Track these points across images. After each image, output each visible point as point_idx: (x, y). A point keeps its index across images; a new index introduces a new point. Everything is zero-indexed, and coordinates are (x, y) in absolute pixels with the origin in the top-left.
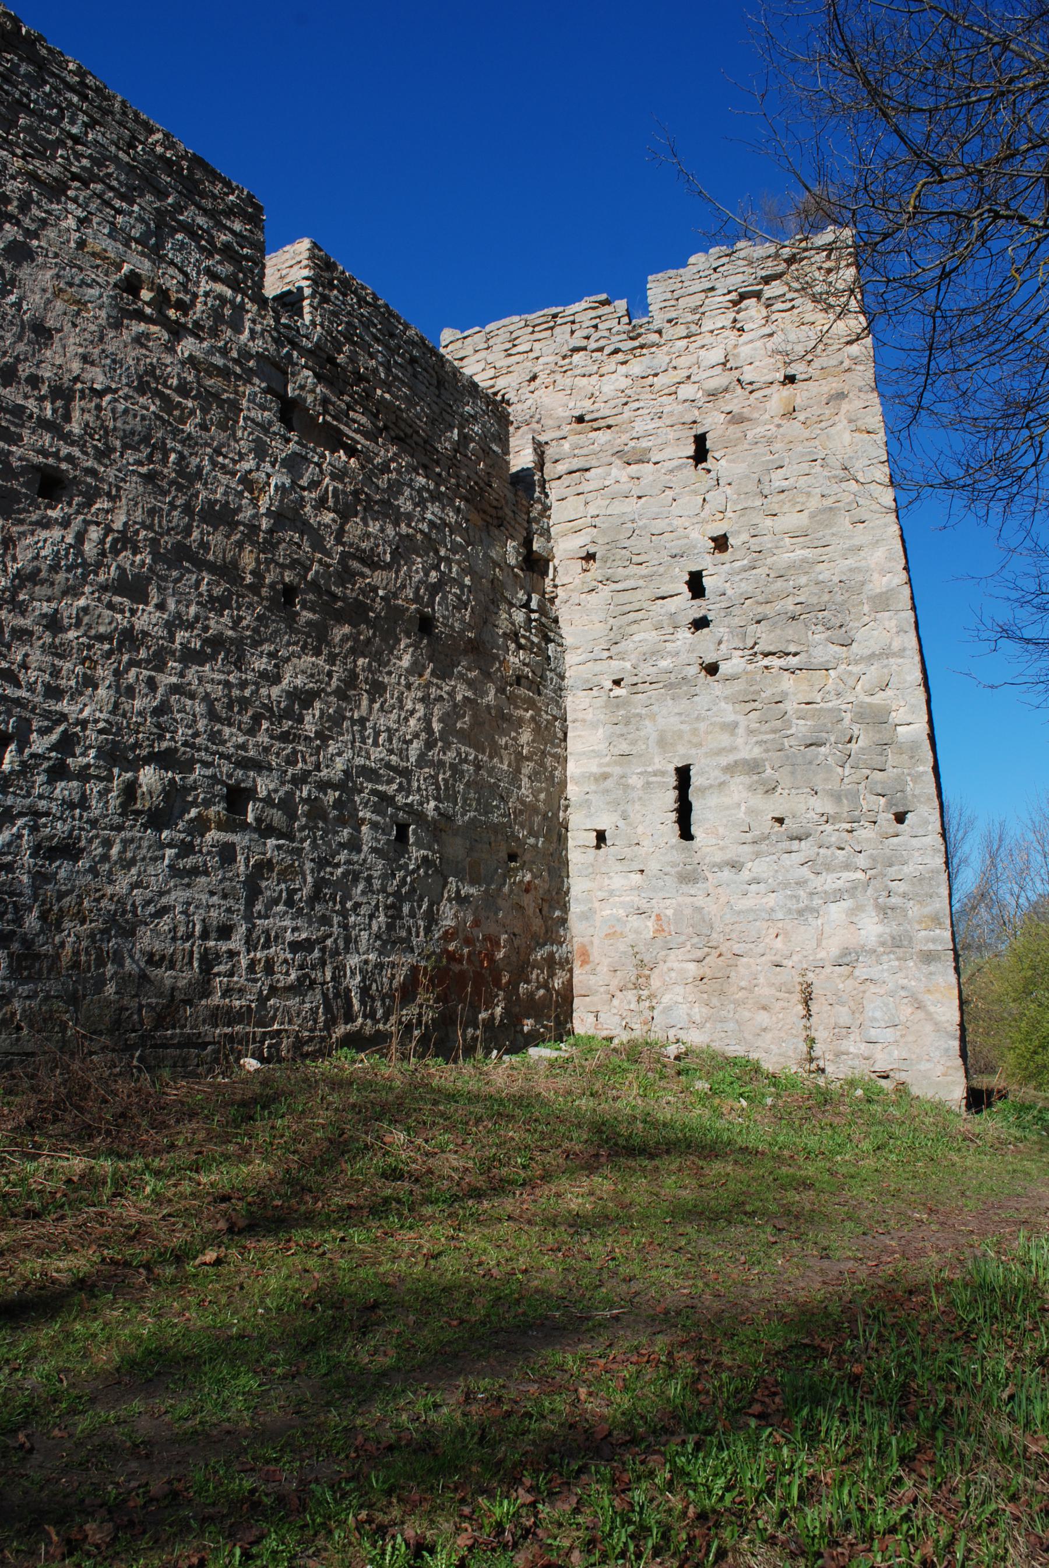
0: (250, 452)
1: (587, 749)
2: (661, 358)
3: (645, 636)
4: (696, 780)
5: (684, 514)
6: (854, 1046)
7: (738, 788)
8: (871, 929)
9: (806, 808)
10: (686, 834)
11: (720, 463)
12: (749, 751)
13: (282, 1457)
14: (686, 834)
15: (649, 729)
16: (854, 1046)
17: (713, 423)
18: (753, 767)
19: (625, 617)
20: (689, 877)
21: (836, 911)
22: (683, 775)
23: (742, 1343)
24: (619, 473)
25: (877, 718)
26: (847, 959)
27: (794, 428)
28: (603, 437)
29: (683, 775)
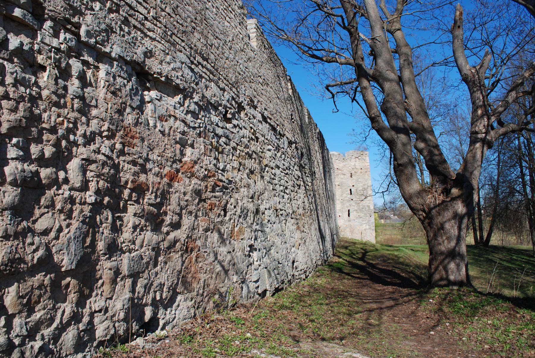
0: (350, 250)
1: (338, 206)
2: (347, 163)
3: (345, 195)
4: (350, 211)
5: (350, 182)
6: (366, 238)
7: (355, 212)
8: (368, 227)
9: (362, 215)
10: (349, 216)
11: (353, 176)
12: (356, 209)
13: (113, 296)
14: (349, 216)
15: (346, 205)
16: (366, 238)
17: (353, 172)
18: (356, 210)
19: (342, 193)
20: (349, 221)
21: (364, 225)
22: (349, 210)
23: (121, 97)
24: (342, 176)
25: (369, 207)
26: (365, 230)
27: (361, 174)
28: (340, 171)
29: (349, 210)
